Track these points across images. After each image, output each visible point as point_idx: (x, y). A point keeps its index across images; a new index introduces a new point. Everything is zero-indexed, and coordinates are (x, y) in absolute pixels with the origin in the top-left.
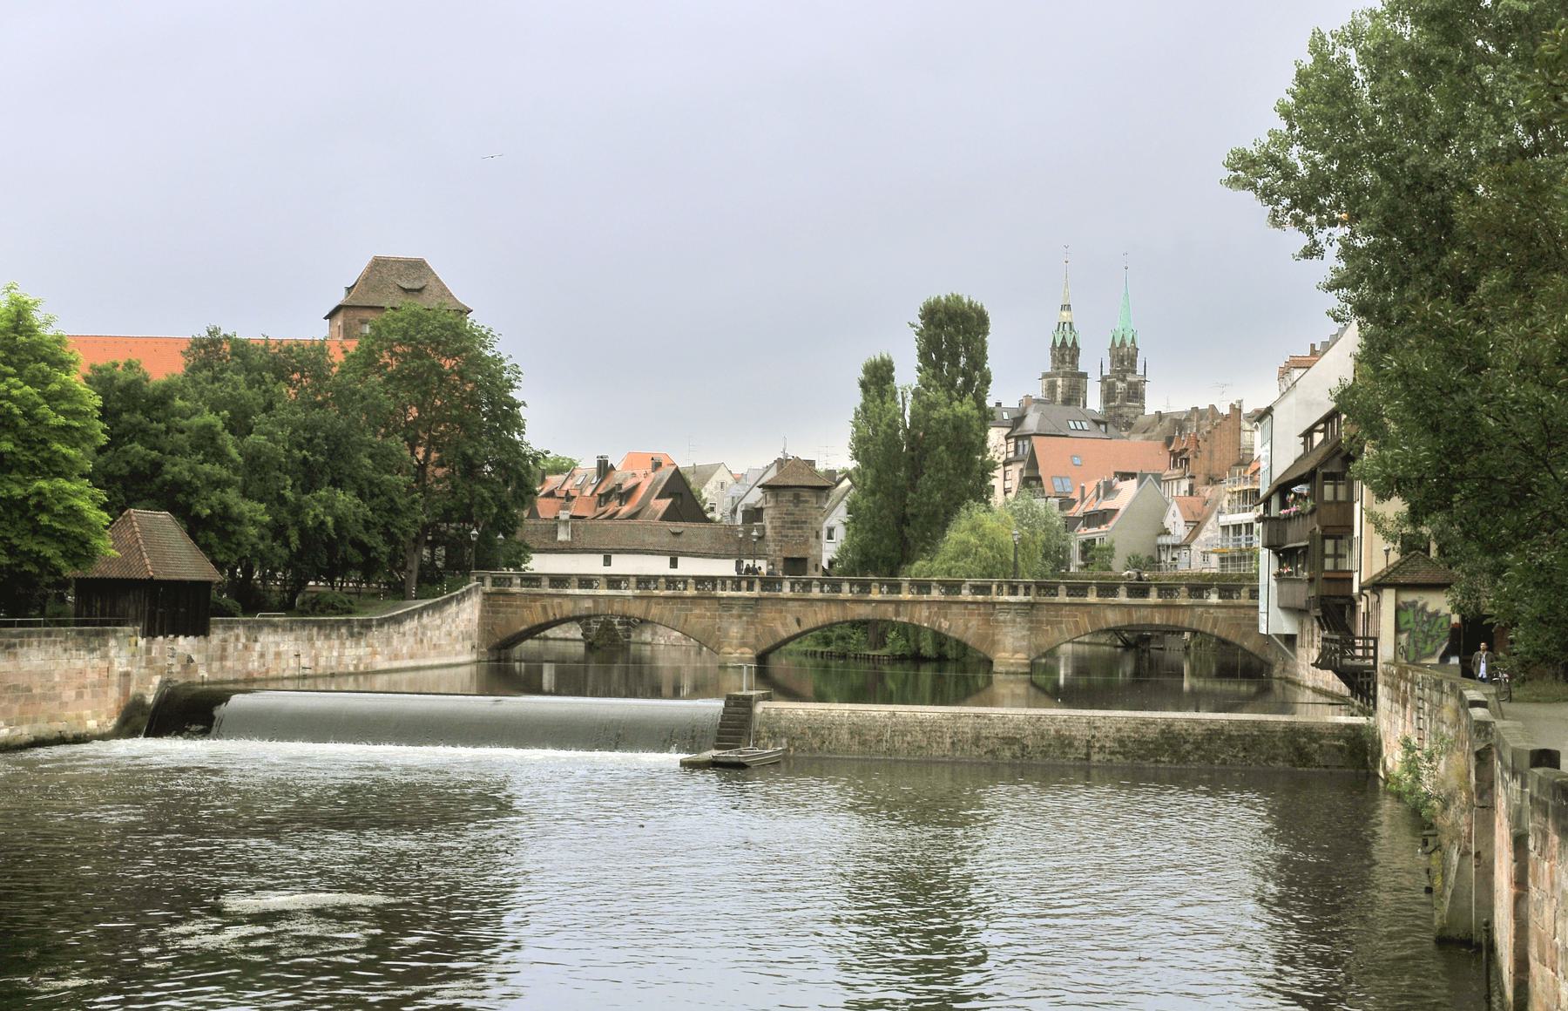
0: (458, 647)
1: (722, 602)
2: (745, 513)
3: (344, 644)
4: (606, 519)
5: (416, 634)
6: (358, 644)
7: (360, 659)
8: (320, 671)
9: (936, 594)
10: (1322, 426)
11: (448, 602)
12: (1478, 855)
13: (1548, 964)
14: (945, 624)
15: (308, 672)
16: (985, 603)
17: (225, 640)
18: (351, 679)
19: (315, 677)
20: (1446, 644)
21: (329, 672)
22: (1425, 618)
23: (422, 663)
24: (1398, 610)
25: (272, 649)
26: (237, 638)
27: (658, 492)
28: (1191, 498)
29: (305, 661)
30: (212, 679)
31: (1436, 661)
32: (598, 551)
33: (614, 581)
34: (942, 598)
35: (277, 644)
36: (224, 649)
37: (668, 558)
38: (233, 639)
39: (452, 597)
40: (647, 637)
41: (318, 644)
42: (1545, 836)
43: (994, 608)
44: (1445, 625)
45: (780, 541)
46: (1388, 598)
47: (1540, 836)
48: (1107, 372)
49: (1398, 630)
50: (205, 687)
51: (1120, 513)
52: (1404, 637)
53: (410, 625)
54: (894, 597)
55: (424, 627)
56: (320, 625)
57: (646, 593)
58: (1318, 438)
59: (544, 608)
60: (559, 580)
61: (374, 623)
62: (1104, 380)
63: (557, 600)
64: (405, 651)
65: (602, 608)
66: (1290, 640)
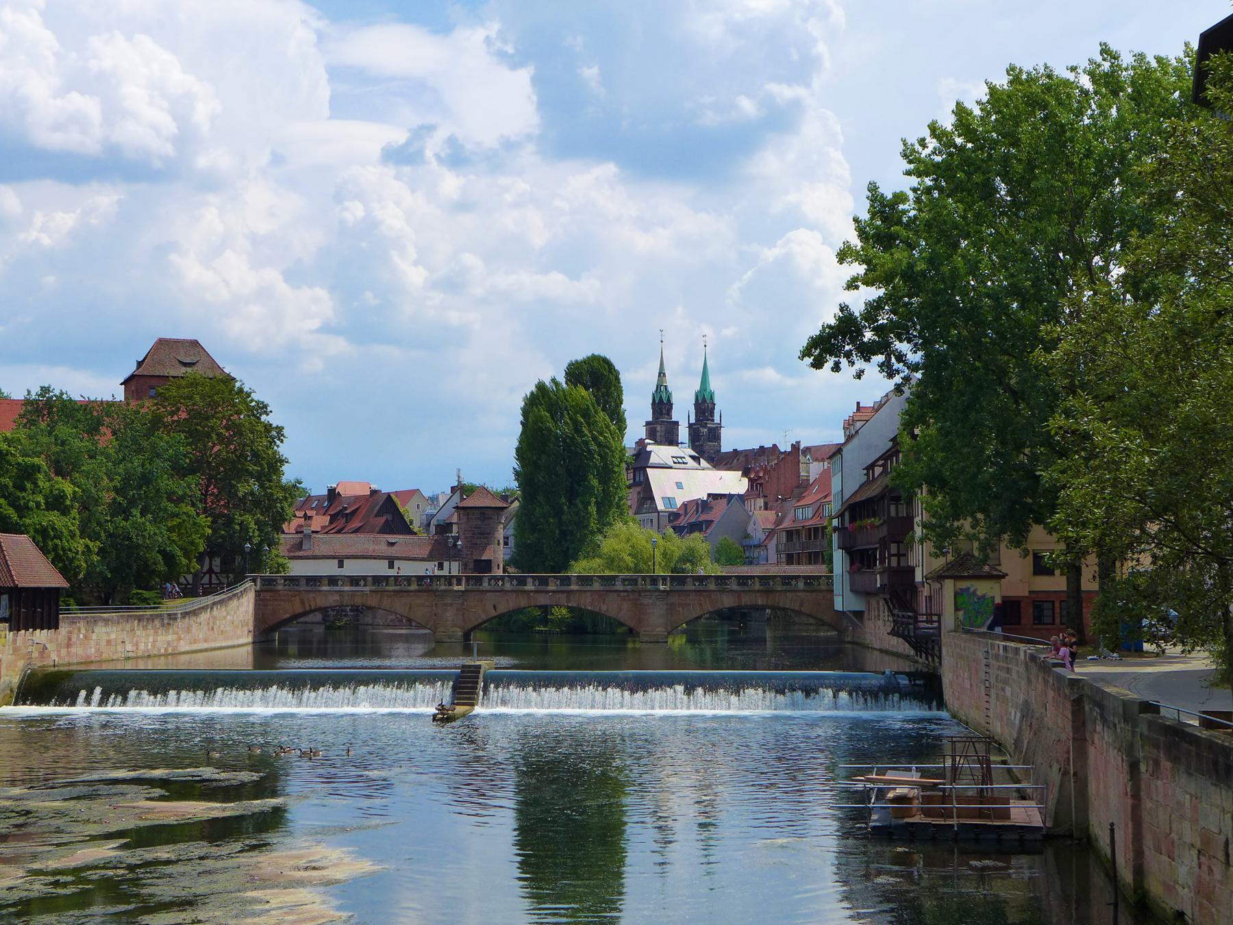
0: (239, 632)
1: (437, 594)
2: (437, 526)
3: (157, 632)
4: (336, 533)
5: (208, 623)
6: (167, 632)
7: (169, 643)
8: (140, 654)
9: (597, 586)
10: (881, 462)
11: (230, 598)
12: (1075, 774)
13: (1163, 851)
14: (604, 608)
15: (130, 654)
16: (633, 591)
17: (70, 632)
18: (162, 658)
19: (137, 658)
20: (992, 618)
21: (146, 654)
22: (976, 600)
23: (213, 645)
24: (956, 594)
25: (105, 638)
26: (79, 630)
27: (375, 512)
28: (767, 512)
29: (129, 647)
30: (61, 662)
31: (984, 630)
32: (334, 557)
33: (354, 580)
34: (601, 588)
35: (108, 633)
36: (70, 639)
37: (387, 561)
38: (76, 631)
39: (234, 595)
40: (369, 619)
41: (138, 633)
42: (1157, 763)
43: (640, 595)
44: (990, 605)
45: (472, 547)
46: (949, 587)
47: (1151, 762)
48: (693, 420)
49: (957, 609)
50: (56, 668)
51: (715, 523)
52: (961, 613)
53: (204, 617)
54: (521, 588)
55: (215, 618)
56: (140, 619)
57: (380, 588)
58: (878, 470)
59: (303, 602)
60: (313, 580)
61: (179, 616)
62: (690, 426)
63: (311, 595)
64: (201, 636)
65: (346, 600)
66: (859, 614)
